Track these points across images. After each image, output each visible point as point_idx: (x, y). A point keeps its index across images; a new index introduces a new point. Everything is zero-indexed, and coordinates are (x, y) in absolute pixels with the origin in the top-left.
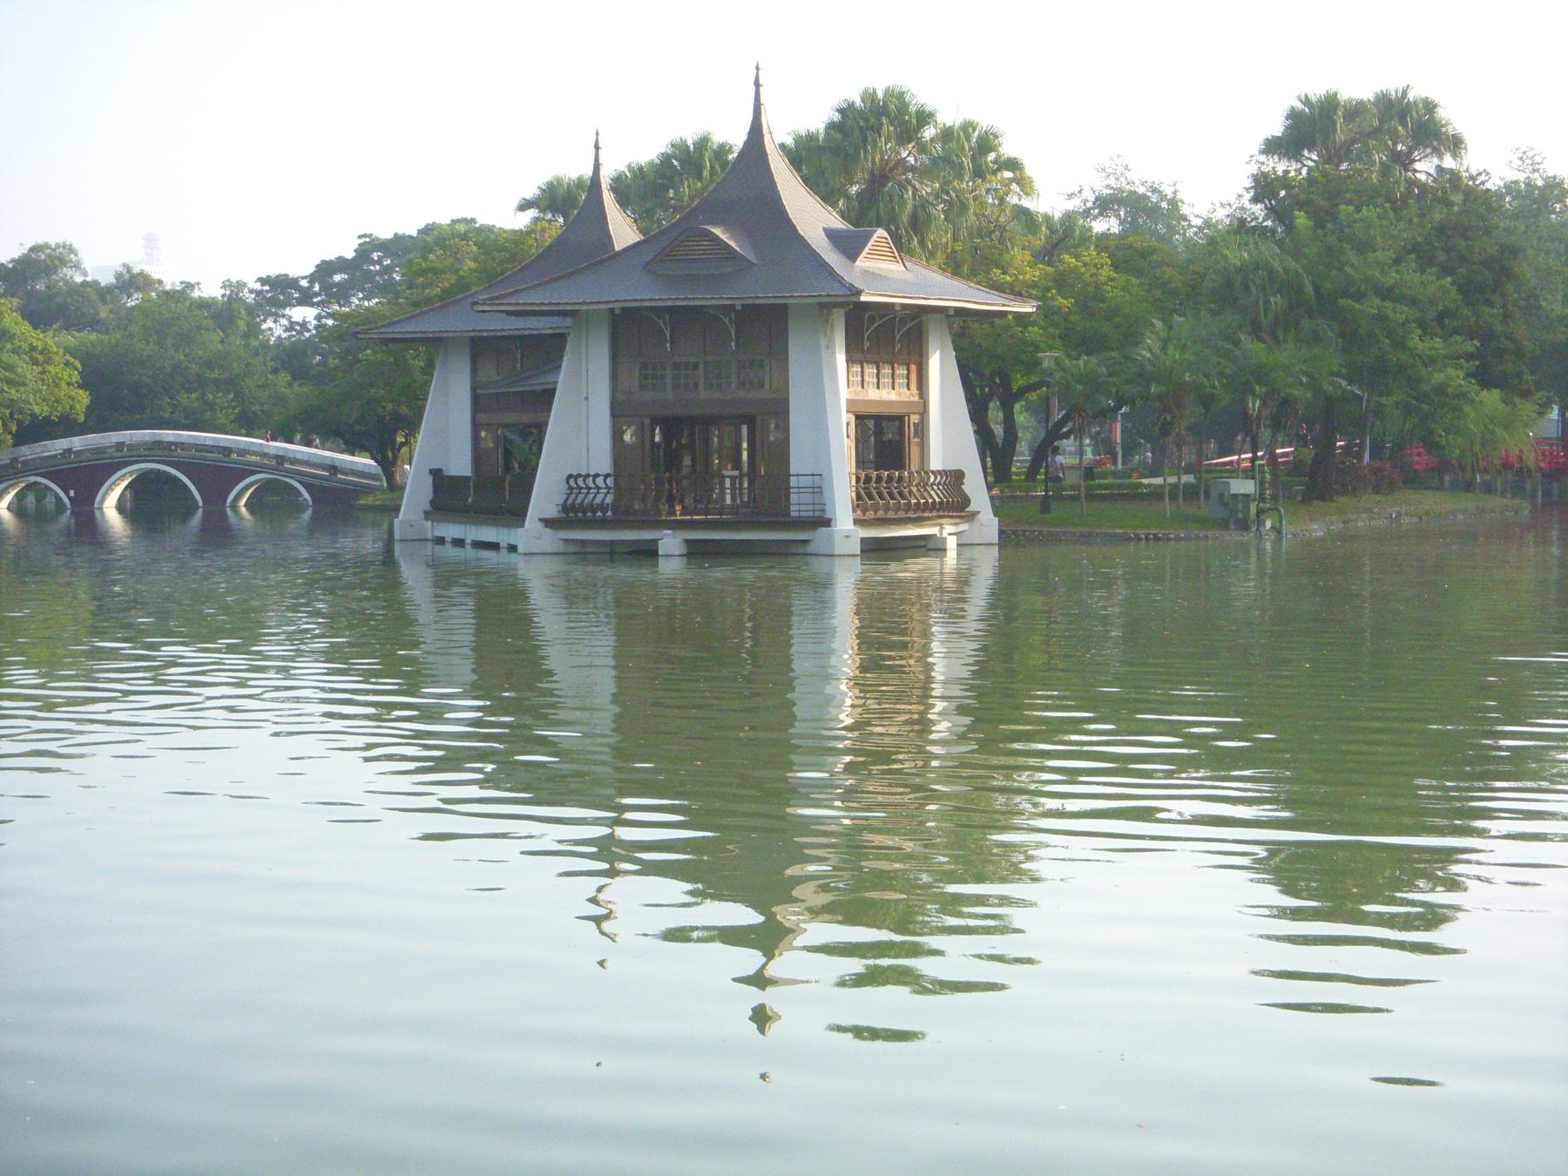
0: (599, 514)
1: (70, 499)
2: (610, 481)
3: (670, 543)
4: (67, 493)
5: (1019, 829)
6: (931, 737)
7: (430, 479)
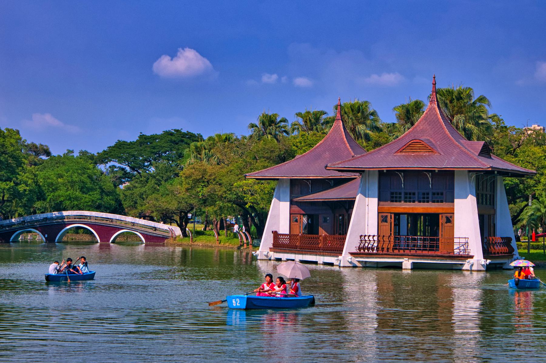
0: (366, 251)
1: (45, 238)
2: (376, 238)
3: (407, 263)
4: (44, 236)
5: (160, 333)
6: (455, 337)
7: (272, 235)
